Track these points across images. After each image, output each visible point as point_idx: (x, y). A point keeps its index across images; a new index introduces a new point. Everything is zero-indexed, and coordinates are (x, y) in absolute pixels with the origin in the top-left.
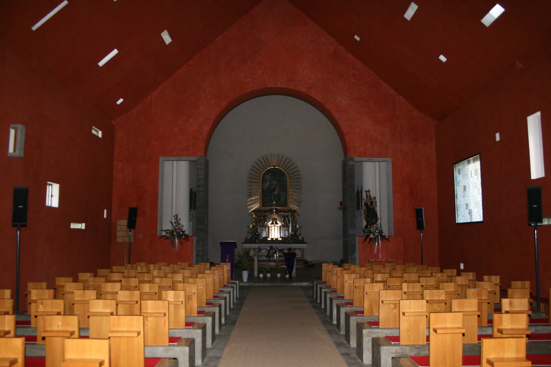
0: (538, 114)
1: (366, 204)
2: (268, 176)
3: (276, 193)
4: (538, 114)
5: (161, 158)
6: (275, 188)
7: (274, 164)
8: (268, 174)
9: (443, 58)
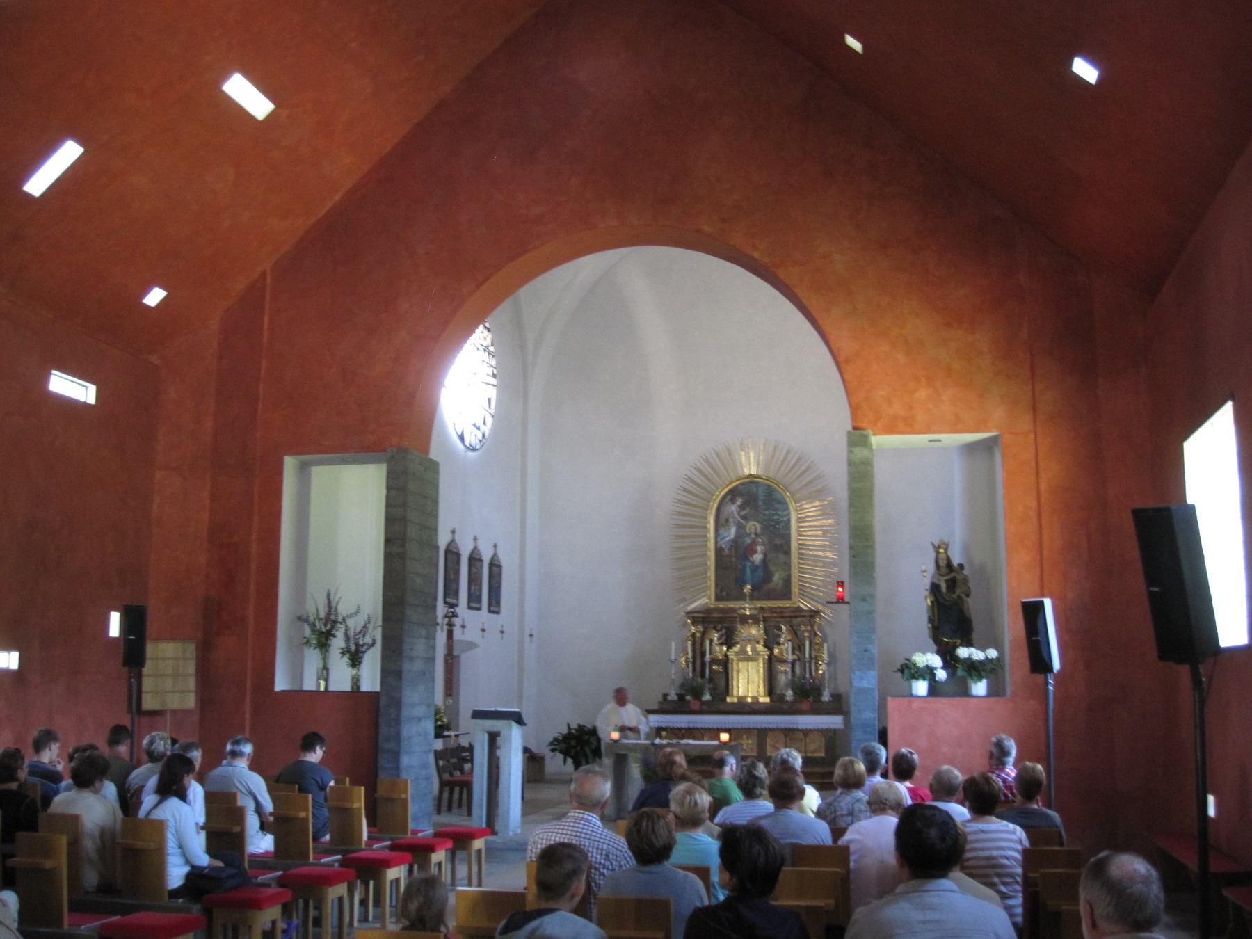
2: (733, 508)
3: (757, 558)
6: (754, 543)
7: (750, 465)
8: (733, 501)
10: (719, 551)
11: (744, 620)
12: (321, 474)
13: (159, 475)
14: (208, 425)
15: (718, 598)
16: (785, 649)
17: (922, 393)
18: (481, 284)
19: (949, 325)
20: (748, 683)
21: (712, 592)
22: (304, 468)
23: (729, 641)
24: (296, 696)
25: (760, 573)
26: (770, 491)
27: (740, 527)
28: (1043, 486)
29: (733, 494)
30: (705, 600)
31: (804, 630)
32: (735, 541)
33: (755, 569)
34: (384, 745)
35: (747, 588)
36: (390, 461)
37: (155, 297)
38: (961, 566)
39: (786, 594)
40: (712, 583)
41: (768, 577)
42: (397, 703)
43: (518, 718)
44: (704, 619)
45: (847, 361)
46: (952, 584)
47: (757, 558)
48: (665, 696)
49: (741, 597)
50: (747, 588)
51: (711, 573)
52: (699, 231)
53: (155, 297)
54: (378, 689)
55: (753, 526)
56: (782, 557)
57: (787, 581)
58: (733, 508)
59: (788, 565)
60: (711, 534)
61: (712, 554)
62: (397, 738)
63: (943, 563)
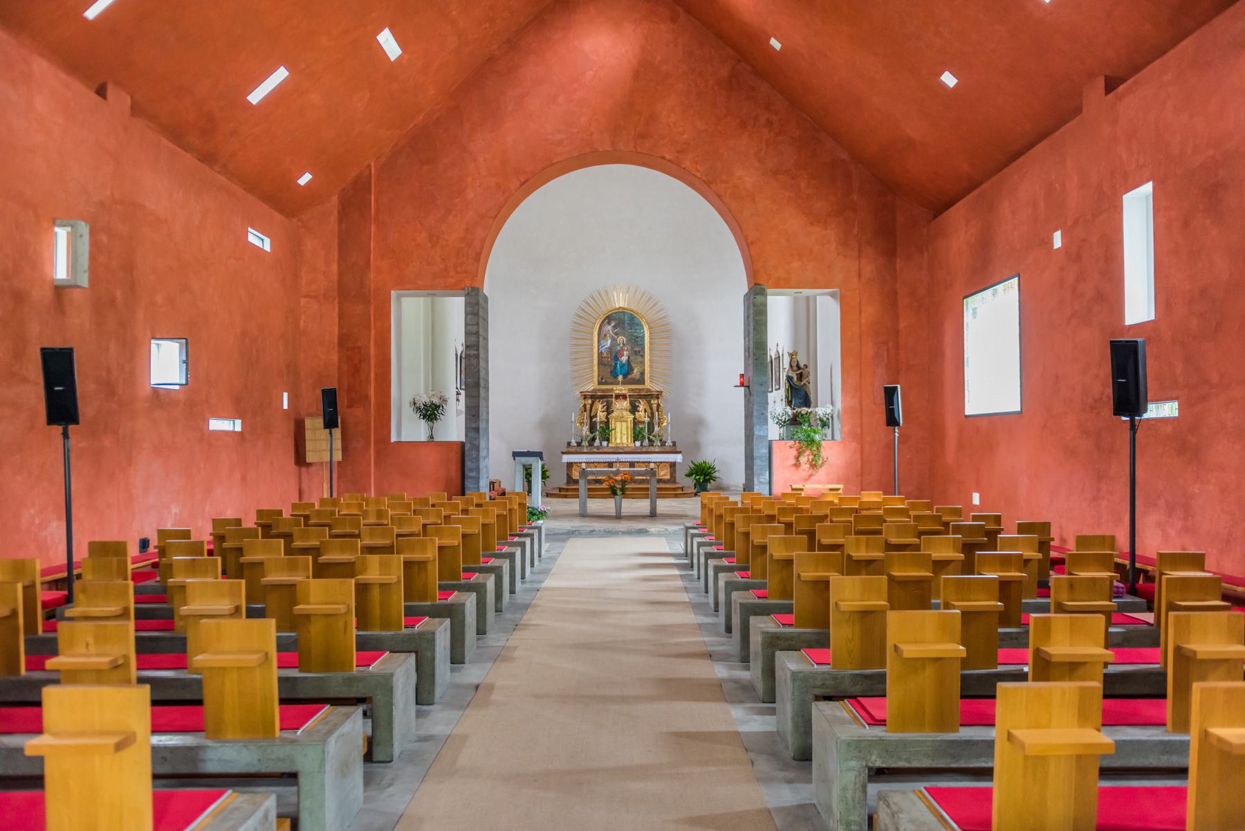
0: (1148, 188)
1: (789, 378)
2: (610, 328)
3: (624, 359)
4: (1148, 188)
5: (393, 293)
6: (622, 350)
7: (620, 301)
8: (609, 323)
9: (949, 79)
10: (600, 354)
11: (618, 397)
12: (405, 300)
13: (303, 301)
14: (335, 267)
15: (599, 383)
16: (642, 415)
17: (796, 264)
18: (522, 184)
19: (812, 224)
20: (621, 434)
21: (596, 380)
22: (399, 297)
23: (609, 411)
24: (399, 443)
25: (626, 368)
26: (632, 318)
27: (613, 340)
28: (863, 321)
29: (609, 319)
30: (591, 386)
31: (654, 402)
32: (610, 349)
33: (622, 366)
34: (468, 474)
35: (620, 378)
36: (467, 295)
37: (305, 179)
38: (806, 366)
39: (641, 381)
40: (596, 374)
41: (630, 370)
42: (477, 448)
43: (539, 455)
44: (594, 397)
45: (752, 243)
46: (800, 377)
47: (624, 359)
48: (569, 444)
49: (617, 383)
50: (620, 378)
51: (596, 368)
52: (663, 158)
53: (305, 179)
54: (463, 439)
55: (621, 339)
56: (640, 359)
57: (642, 374)
58: (610, 328)
59: (643, 363)
60: (596, 344)
61: (596, 356)
62: (478, 469)
63: (794, 365)
